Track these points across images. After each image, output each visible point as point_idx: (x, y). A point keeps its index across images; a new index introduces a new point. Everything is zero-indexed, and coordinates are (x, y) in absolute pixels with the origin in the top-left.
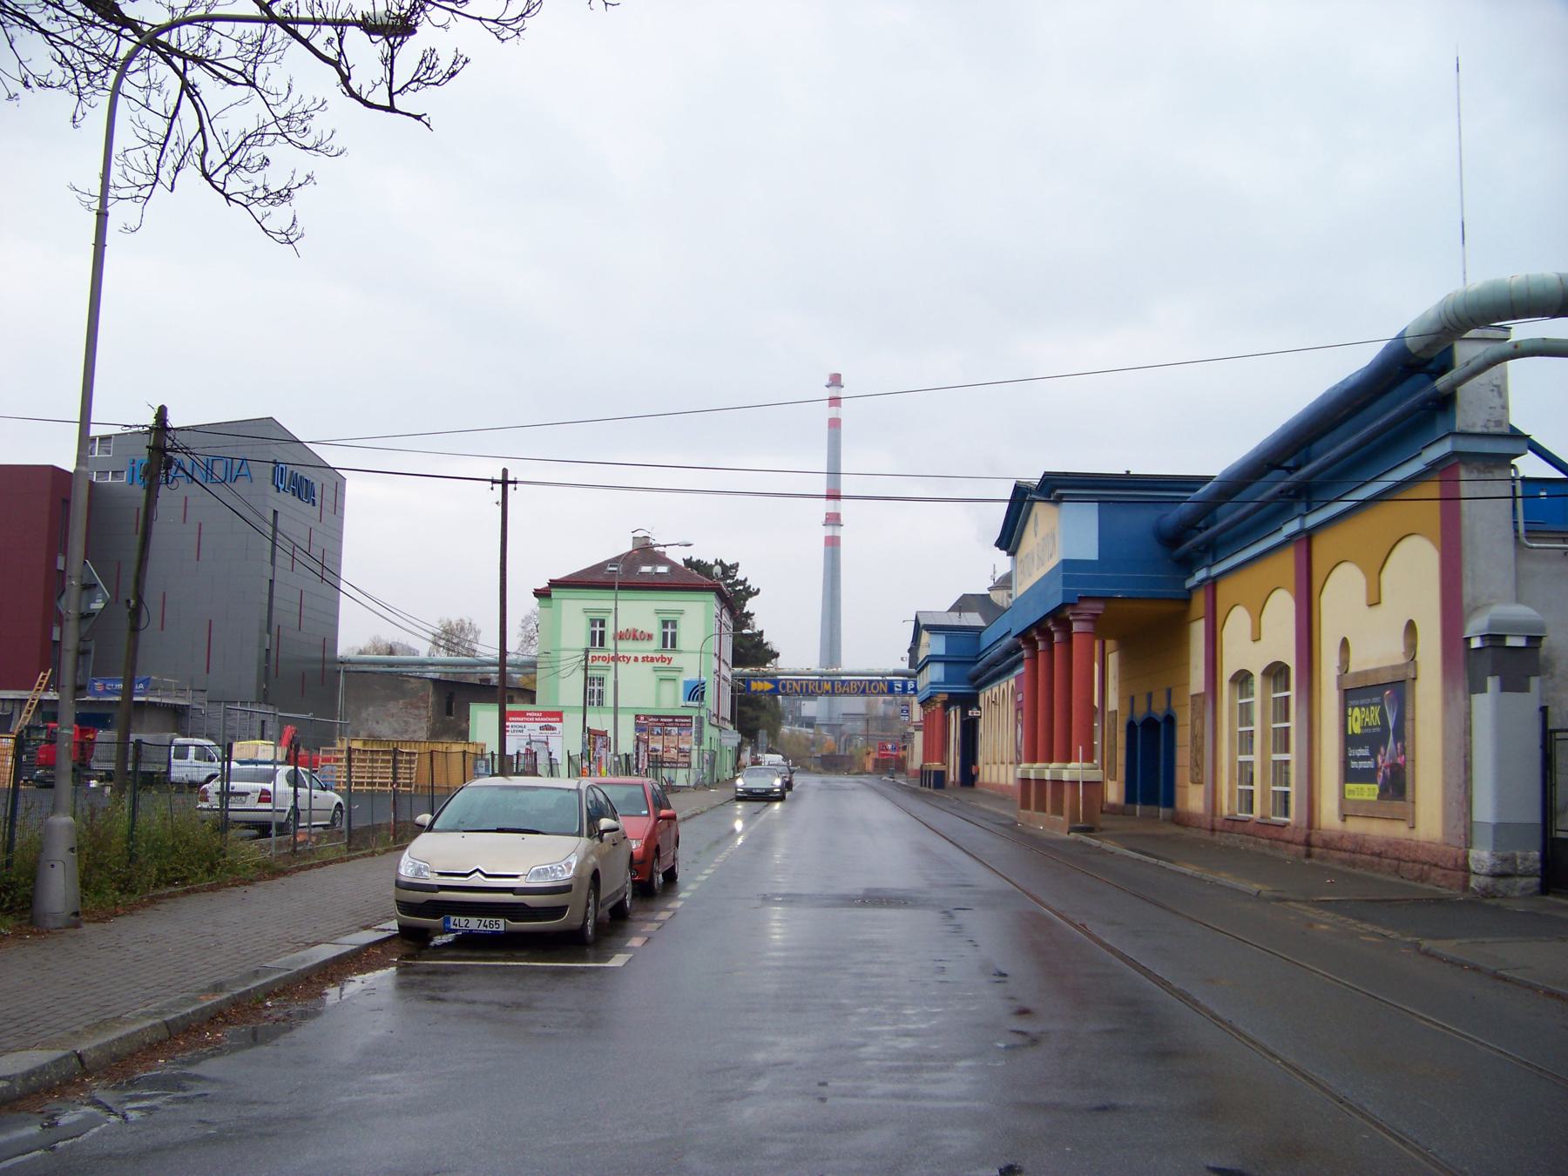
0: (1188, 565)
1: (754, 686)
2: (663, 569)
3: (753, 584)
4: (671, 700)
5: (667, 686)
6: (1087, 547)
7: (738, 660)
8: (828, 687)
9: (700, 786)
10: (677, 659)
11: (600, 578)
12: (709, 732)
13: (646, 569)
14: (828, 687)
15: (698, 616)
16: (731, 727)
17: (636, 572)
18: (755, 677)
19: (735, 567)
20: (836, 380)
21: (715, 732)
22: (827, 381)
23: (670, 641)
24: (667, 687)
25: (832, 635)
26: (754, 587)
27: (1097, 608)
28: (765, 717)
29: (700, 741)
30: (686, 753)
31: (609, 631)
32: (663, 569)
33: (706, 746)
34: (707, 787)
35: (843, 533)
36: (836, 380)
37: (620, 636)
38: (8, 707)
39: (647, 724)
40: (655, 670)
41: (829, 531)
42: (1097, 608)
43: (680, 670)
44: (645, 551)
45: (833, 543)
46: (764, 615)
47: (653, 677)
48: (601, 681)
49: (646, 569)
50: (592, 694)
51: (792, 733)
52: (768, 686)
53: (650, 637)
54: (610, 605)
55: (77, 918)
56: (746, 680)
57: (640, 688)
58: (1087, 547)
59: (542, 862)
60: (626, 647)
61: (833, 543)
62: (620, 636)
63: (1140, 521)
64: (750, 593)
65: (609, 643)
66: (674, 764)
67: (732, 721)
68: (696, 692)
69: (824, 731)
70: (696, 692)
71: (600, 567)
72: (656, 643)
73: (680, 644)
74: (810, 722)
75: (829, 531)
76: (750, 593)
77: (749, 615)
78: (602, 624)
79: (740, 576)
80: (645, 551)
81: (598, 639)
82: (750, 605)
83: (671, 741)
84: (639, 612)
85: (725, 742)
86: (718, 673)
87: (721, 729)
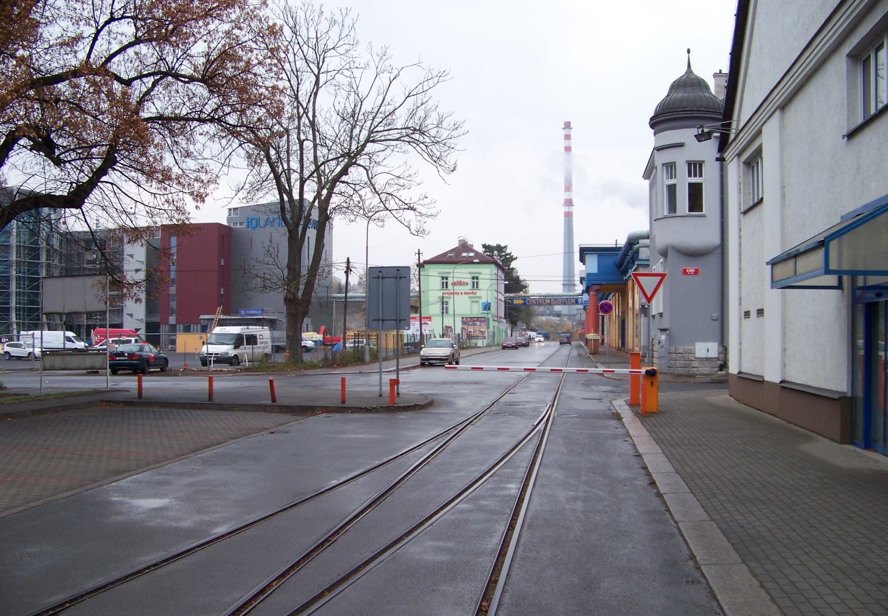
0: (625, 272)
1: (515, 302)
2: (472, 254)
3: (514, 255)
4: (477, 310)
5: (475, 305)
6: (594, 269)
7: (508, 289)
8: (548, 301)
9: (488, 345)
10: (479, 293)
11: (445, 259)
12: (492, 323)
13: (464, 254)
14: (548, 301)
15: (487, 273)
16: (504, 321)
17: (459, 256)
18: (515, 298)
19: (506, 247)
20: (568, 125)
21: (496, 324)
22: (563, 126)
23: (475, 285)
24: (475, 305)
25: (569, 266)
26: (515, 256)
27: (598, 287)
28: (523, 315)
29: (488, 328)
30: (483, 333)
31: (450, 281)
32: (472, 254)
33: (491, 329)
34: (491, 346)
35: (574, 210)
36: (568, 125)
37: (454, 284)
38: (206, 322)
39: (468, 321)
40: (470, 298)
41: (567, 209)
42: (598, 287)
43: (480, 298)
44: (465, 246)
45: (568, 216)
46: (521, 268)
47: (469, 301)
48: (447, 303)
49: (464, 254)
50: (444, 311)
51: (547, 320)
52: (521, 302)
53: (467, 284)
54: (451, 270)
55: (370, 362)
56: (512, 299)
57: (463, 306)
58: (594, 269)
59: (444, 352)
60: (457, 288)
61: (568, 216)
62: (454, 284)
63: (611, 261)
64: (512, 259)
65: (450, 287)
66: (477, 337)
67: (505, 318)
68: (487, 307)
69: (565, 319)
70: (487, 307)
71: (445, 254)
72: (470, 286)
73: (480, 286)
74: (558, 315)
75: (567, 209)
76: (512, 259)
77: (513, 269)
78: (447, 278)
79: (508, 251)
80: (465, 246)
81: (445, 285)
82: (513, 265)
83: (477, 328)
84: (462, 273)
85: (501, 327)
86: (497, 298)
87: (499, 322)
